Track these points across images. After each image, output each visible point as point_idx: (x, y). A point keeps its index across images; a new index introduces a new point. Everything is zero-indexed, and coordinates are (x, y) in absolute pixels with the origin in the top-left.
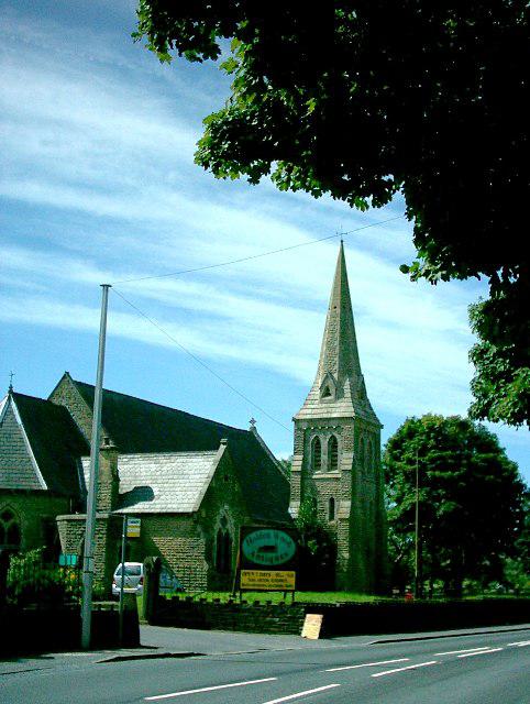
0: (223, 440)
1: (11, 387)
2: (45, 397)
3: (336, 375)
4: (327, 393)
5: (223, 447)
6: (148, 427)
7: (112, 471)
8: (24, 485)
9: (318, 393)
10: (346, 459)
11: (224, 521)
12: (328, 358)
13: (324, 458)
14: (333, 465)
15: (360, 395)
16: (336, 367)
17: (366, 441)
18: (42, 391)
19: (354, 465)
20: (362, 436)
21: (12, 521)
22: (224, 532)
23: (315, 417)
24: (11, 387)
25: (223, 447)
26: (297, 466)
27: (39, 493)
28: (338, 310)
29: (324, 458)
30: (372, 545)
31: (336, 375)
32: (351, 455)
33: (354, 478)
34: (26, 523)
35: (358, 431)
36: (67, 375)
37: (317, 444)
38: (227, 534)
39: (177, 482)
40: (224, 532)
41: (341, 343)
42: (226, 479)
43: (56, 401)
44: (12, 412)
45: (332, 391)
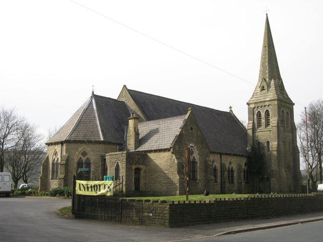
0: (190, 108)
1: (93, 92)
2: (116, 98)
3: (267, 79)
4: (263, 89)
5: (189, 112)
6: (155, 107)
7: (135, 129)
8: (93, 139)
9: (259, 89)
10: (274, 121)
11: (190, 153)
12: (262, 72)
13: (263, 121)
14: (267, 124)
15: (280, 88)
16: (267, 75)
17: (285, 112)
18: (114, 95)
19: (278, 123)
20: (282, 109)
21: (87, 157)
22: (231, 167)
23: (257, 101)
24: (93, 92)
25: (189, 112)
26: (251, 126)
27: (99, 142)
28: (267, 48)
29: (263, 121)
30: (292, 165)
31: (267, 79)
32: (276, 118)
33: (278, 130)
34: (94, 157)
35: (279, 106)
36: (125, 86)
37: (259, 114)
38: (232, 168)
39: (169, 129)
40: (231, 167)
41: (269, 63)
42: (192, 129)
43: (121, 100)
44: (92, 104)
45: (266, 87)
